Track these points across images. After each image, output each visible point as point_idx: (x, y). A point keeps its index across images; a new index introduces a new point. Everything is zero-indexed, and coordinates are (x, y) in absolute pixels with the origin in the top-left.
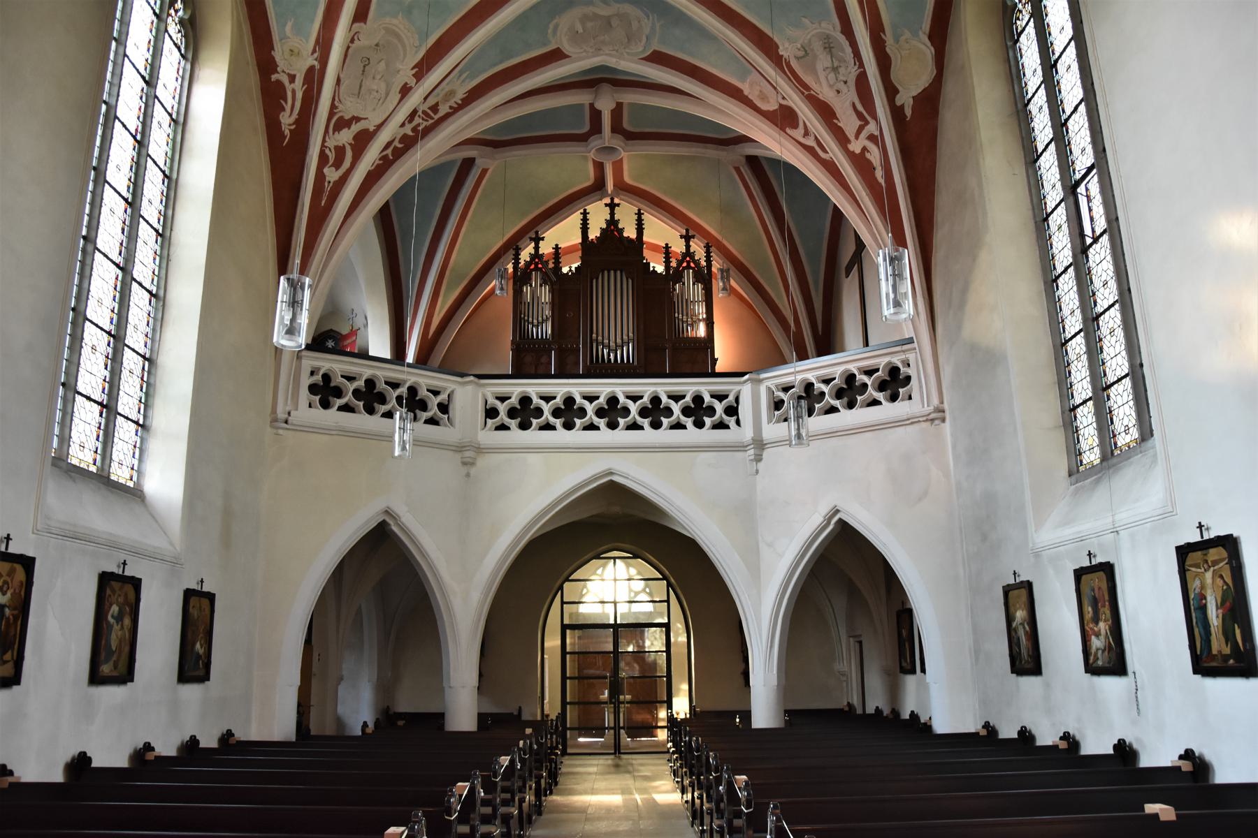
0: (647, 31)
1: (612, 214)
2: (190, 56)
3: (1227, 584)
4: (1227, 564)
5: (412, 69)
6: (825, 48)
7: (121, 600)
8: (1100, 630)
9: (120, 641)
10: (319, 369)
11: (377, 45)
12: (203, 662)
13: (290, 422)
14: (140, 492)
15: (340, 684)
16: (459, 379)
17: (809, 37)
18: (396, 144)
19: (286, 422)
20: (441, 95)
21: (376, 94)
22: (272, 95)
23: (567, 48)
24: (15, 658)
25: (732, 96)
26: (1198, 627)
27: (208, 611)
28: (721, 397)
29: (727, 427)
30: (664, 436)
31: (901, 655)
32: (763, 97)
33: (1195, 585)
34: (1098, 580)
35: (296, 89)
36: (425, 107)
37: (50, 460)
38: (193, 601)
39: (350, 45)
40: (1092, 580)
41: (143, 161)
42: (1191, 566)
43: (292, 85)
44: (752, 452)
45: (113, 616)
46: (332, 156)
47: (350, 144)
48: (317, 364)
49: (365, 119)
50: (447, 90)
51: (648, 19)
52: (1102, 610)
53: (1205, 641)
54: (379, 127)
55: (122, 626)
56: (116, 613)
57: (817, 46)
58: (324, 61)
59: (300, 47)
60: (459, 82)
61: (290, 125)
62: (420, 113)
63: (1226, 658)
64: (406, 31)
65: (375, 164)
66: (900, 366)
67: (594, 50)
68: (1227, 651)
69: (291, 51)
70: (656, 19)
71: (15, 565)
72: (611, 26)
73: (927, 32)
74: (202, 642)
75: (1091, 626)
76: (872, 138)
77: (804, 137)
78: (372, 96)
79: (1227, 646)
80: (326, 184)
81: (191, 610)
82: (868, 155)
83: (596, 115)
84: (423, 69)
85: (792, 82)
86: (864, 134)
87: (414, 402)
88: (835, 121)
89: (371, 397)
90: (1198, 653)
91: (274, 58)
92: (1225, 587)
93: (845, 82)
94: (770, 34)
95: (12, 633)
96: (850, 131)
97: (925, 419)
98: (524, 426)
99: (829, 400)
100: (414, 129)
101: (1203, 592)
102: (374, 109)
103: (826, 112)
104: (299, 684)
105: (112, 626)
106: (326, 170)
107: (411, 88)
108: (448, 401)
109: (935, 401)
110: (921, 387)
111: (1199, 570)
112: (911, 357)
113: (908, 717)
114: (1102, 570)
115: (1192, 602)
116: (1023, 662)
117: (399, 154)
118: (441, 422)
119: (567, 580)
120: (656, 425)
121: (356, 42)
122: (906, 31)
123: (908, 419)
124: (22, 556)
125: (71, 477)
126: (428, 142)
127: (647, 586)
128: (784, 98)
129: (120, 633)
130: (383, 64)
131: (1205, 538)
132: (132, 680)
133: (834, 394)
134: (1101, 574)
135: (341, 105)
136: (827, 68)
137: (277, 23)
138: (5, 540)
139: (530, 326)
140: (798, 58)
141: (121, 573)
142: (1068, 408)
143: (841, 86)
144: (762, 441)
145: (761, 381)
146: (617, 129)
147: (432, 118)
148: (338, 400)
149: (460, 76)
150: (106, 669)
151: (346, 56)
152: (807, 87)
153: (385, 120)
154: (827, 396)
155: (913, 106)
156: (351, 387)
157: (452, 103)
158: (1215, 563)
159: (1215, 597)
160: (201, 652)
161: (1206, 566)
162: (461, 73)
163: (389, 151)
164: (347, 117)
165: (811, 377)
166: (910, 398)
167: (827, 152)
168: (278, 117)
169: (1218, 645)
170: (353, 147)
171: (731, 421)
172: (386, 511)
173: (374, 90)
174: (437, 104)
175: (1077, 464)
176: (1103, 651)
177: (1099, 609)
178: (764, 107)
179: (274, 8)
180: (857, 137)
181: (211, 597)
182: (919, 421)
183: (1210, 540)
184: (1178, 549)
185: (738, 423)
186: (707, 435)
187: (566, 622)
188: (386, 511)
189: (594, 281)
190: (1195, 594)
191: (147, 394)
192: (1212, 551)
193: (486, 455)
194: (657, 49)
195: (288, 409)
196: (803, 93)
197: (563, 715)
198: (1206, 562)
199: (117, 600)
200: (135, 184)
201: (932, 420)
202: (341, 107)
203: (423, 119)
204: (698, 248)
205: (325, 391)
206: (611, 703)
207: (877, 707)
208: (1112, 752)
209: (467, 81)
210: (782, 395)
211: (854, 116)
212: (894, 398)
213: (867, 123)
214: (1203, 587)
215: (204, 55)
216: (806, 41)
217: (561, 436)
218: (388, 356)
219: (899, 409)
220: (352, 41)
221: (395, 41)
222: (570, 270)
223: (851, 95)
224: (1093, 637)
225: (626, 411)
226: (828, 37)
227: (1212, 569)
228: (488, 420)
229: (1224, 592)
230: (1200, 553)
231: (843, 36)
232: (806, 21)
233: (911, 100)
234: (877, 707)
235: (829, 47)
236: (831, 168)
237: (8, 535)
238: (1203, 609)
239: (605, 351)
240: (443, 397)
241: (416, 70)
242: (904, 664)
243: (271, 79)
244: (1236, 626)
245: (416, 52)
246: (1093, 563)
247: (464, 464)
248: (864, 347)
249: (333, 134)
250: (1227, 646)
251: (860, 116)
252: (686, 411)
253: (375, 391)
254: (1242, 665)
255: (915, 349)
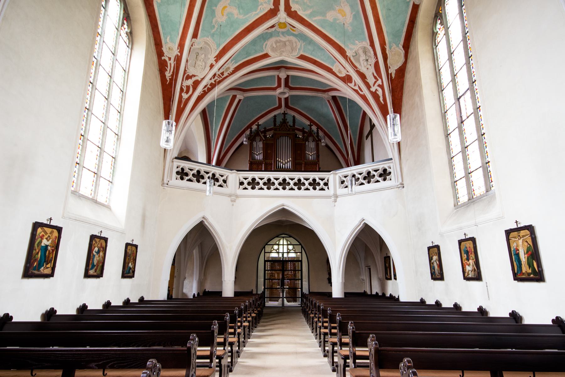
0: (299, 47)
1: (285, 117)
2: (130, 46)
3: (529, 245)
4: (529, 236)
5: (214, 58)
6: (364, 52)
7: (99, 245)
8: (470, 263)
9: (98, 261)
10: (180, 166)
11: (201, 48)
12: (132, 270)
13: (168, 184)
14: (109, 207)
15: (184, 280)
16: (230, 171)
17: (357, 48)
18: (209, 86)
19: (167, 184)
20: (224, 69)
21: (201, 67)
22: (162, 66)
23: (270, 53)
24: (52, 266)
25: (329, 71)
26: (515, 262)
27: (135, 252)
28: (322, 179)
29: (324, 190)
30: (302, 192)
31: (386, 273)
32: (340, 72)
33: (514, 246)
34: (470, 244)
35: (171, 63)
36: (219, 73)
37: (70, 191)
38: (129, 247)
39: (191, 47)
40: (466, 244)
41: (111, 84)
42: (512, 238)
43: (170, 61)
44: (333, 198)
45: (95, 252)
46: (185, 89)
47: (192, 85)
48: (179, 164)
49: (197, 76)
50: (227, 67)
51: (299, 42)
52: (471, 255)
53: (519, 267)
54: (203, 79)
55: (99, 255)
56: (97, 251)
57: (361, 52)
58: (181, 51)
59: (173, 47)
60: (231, 64)
61: (169, 76)
62: (217, 75)
63: (529, 274)
64: (212, 43)
65: (201, 93)
66: (387, 168)
67: (279, 54)
68: (530, 271)
69: (169, 48)
70: (302, 42)
71: (53, 230)
72: (286, 45)
73: (402, 44)
74: (132, 263)
75: (466, 261)
76: (379, 86)
77: (354, 86)
78: (200, 67)
79: (530, 269)
80: (183, 99)
81: (128, 251)
82: (377, 92)
83: (279, 79)
84: (219, 57)
85: (351, 65)
86: (377, 84)
87: (214, 178)
88: (366, 80)
89: (199, 177)
90: (516, 272)
91: (163, 50)
92: (528, 246)
93: (370, 65)
94: (344, 47)
95: (51, 256)
96: (371, 84)
97: (396, 187)
98: (253, 188)
99: (361, 180)
100: (215, 81)
101: (518, 248)
102: (200, 72)
103: (363, 76)
104: (169, 279)
105: (95, 256)
106: (183, 94)
107: (214, 65)
108: (226, 179)
109: (400, 181)
110: (395, 176)
111: (516, 239)
112: (391, 165)
113: (389, 296)
114: (471, 240)
115: (512, 252)
116: (436, 276)
117: (209, 90)
118: (224, 186)
119: (267, 244)
120: (299, 189)
121: (193, 46)
122: (394, 44)
123: (390, 187)
124: (56, 226)
125: (80, 199)
126: (220, 86)
127: (294, 248)
128: (348, 72)
129: (98, 258)
130: (203, 56)
131: (466, 238)
132: (134, 277)
133: (363, 178)
134: (471, 241)
135: (188, 70)
136: (364, 60)
137: (164, 37)
138: (50, 220)
139: (255, 155)
140: (353, 56)
141: (99, 235)
142: (454, 181)
143: (369, 66)
144: (337, 195)
145: (336, 174)
146: (287, 85)
147: (221, 77)
148: (187, 177)
149: (232, 62)
150: (91, 272)
151: (190, 51)
152: (356, 67)
153: (205, 76)
154: (360, 179)
155: (395, 73)
156: (192, 173)
157: (228, 72)
158: (523, 236)
159: (524, 250)
160: (131, 267)
161: (519, 238)
162: (232, 61)
163: (206, 89)
164: (190, 75)
165: (355, 172)
166: (391, 180)
167: (362, 92)
168: (165, 73)
169: (525, 269)
170: (193, 86)
171: (326, 188)
172: (203, 217)
173: (200, 65)
174: (223, 72)
175: (457, 202)
176: (472, 271)
177: (469, 255)
178: (340, 75)
179: (162, 31)
180: (374, 85)
181: (136, 246)
182: (394, 188)
183: (468, 239)
184: (506, 231)
185: (328, 188)
186: (317, 192)
187: (266, 259)
188: (203, 217)
189: (278, 140)
190: (514, 249)
191: (113, 171)
192: (522, 231)
193: (240, 198)
194: (302, 54)
195: (168, 180)
196: (355, 70)
197: (264, 292)
198: (519, 236)
199: (97, 245)
200: (109, 92)
201: (399, 187)
202: (188, 71)
203: (218, 77)
204: (314, 128)
205: (182, 174)
206: (281, 288)
207: (377, 292)
208: (453, 307)
209: (234, 64)
210: (344, 179)
211: (373, 78)
212: (385, 180)
213: (378, 80)
214: (517, 246)
215: (135, 47)
216: (357, 50)
217: (266, 192)
218: (205, 162)
219: (387, 183)
220: (192, 46)
221: (208, 47)
222: (270, 136)
223: (372, 70)
224: (467, 266)
225: (289, 184)
226: (365, 48)
227: (522, 239)
228: (240, 186)
229: (528, 248)
230: (516, 232)
231: (371, 47)
232: (357, 42)
233: (395, 71)
234: (377, 292)
235: (365, 52)
236: (364, 98)
237: (51, 218)
238: (518, 255)
239: (281, 164)
240: (224, 178)
241: (216, 58)
242: (387, 276)
243: (161, 59)
244: (534, 261)
245: (216, 52)
246: (433, 245)
247: (232, 201)
248: (372, 162)
249: (185, 81)
250: (530, 269)
251: (375, 77)
252: (310, 184)
253: (200, 175)
254: (537, 277)
255: (393, 162)
